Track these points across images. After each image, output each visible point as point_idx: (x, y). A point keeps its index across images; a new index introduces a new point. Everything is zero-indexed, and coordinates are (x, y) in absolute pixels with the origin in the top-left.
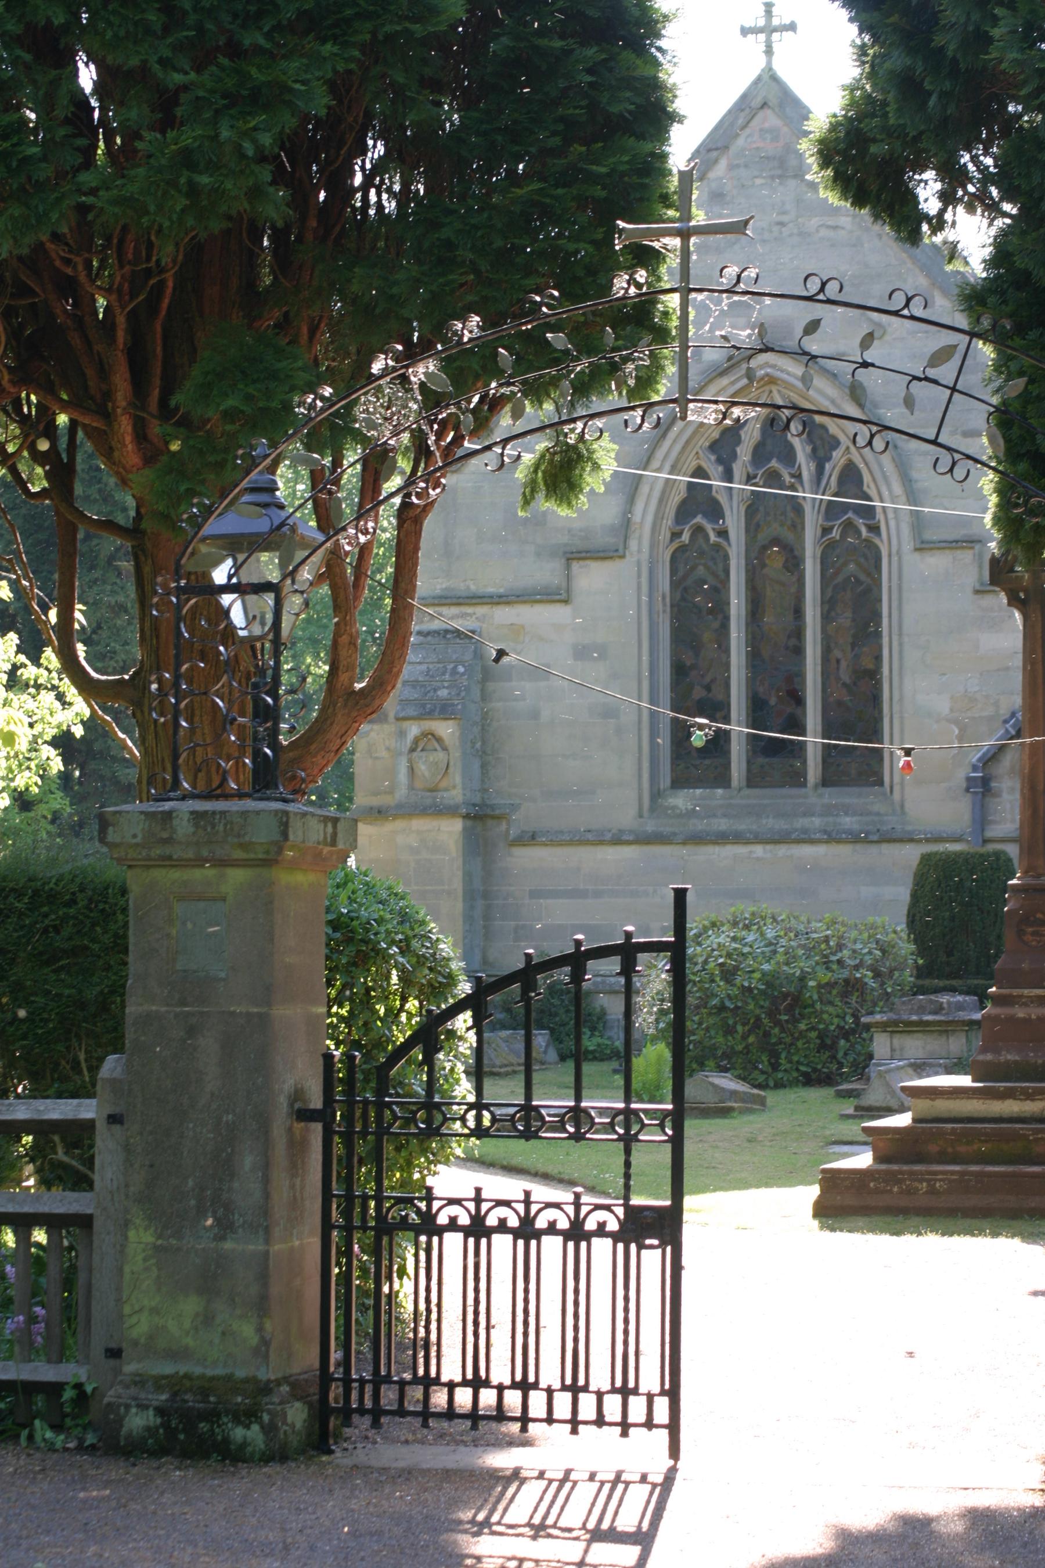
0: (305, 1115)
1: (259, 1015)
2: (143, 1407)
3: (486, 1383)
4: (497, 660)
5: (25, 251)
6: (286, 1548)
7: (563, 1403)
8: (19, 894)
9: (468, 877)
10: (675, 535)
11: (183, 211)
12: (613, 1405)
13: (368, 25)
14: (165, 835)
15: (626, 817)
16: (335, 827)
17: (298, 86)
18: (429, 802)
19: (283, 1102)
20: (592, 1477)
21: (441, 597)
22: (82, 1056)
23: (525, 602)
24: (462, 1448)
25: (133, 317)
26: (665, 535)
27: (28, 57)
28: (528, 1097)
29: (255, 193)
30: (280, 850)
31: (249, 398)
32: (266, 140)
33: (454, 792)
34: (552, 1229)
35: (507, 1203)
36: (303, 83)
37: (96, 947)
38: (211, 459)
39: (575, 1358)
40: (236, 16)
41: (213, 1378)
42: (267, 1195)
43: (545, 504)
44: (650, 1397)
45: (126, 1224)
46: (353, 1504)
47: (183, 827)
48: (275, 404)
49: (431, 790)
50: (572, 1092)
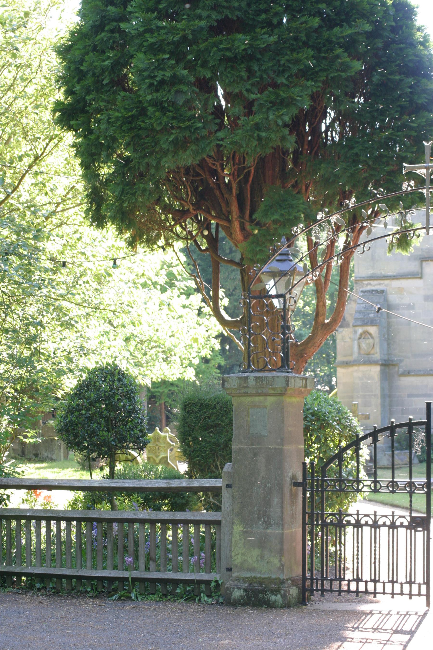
0: (296, 484)
1: (279, 449)
2: (239, 588)
3: (361, 580)
4: (378, 312)
5: (198, 162)
6: (286, 635)
7: (388, 587)
8: (195, 405)
9: (382, 389)
11: (256, 146)
12: (406, 588)
13: (325, 74)
14: (245, 385)
16: (306, 381)
17: (298, 98)
18: (366, 359)
19: (288, 480)
20: (398, 613)
22: (218, 464)
23: (404, 278)
24: (354, 604)
25: (239, 183)
27: (197, 90)
28: (393, 477)
29: (283, 138)
30: (286, 390)
31: (282, 215)
32: (287, 119)
33: (376, 355)
34: (384, 525)
35: (368, 516)
36: (301, 96)
37: (223, 424)
38: (269, 238)
39: (393, 571)
40: (275, 72)
41: (264, 578)
42: (282, 513)
43: (397, 251)
44: (420, 585)
45: (233, 523)
46: (312, 622)
47: (251, 382)
48: (292, 217)
49: (368, 354)
50: (425, 475)
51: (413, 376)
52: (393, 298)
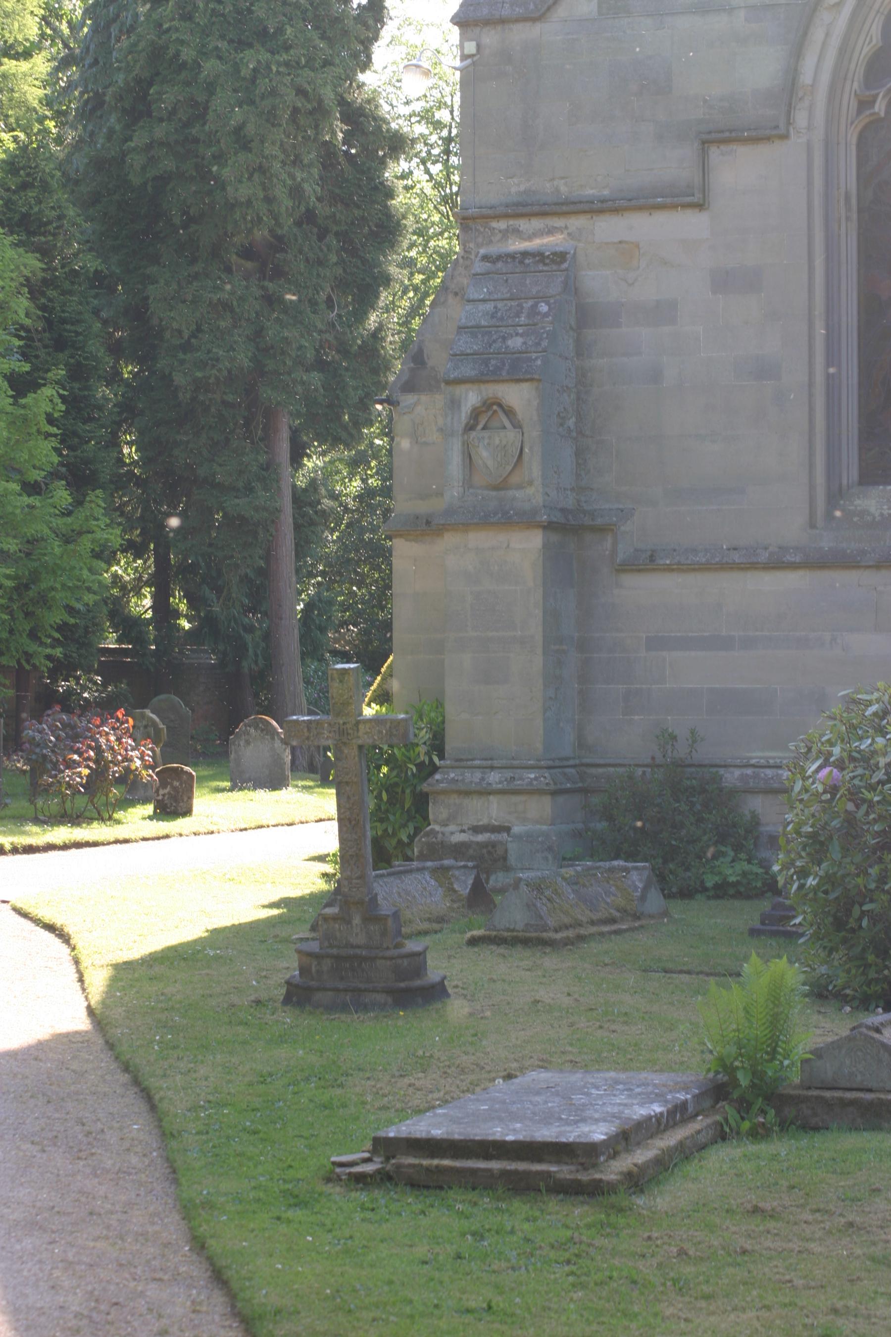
9: (552, 617)
10: (864, 104)
15: (790, 528)
21: (517, 204)
26: (848, 103)
33: (530, 491)
51: (669, 569)
52: (600, 282)
